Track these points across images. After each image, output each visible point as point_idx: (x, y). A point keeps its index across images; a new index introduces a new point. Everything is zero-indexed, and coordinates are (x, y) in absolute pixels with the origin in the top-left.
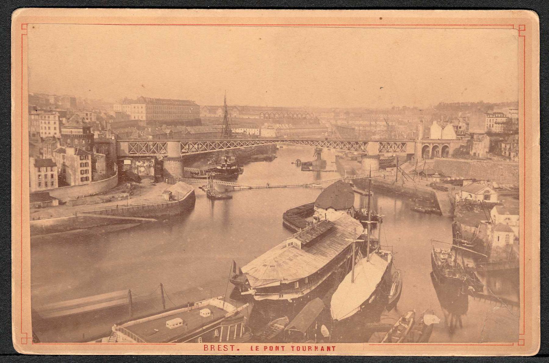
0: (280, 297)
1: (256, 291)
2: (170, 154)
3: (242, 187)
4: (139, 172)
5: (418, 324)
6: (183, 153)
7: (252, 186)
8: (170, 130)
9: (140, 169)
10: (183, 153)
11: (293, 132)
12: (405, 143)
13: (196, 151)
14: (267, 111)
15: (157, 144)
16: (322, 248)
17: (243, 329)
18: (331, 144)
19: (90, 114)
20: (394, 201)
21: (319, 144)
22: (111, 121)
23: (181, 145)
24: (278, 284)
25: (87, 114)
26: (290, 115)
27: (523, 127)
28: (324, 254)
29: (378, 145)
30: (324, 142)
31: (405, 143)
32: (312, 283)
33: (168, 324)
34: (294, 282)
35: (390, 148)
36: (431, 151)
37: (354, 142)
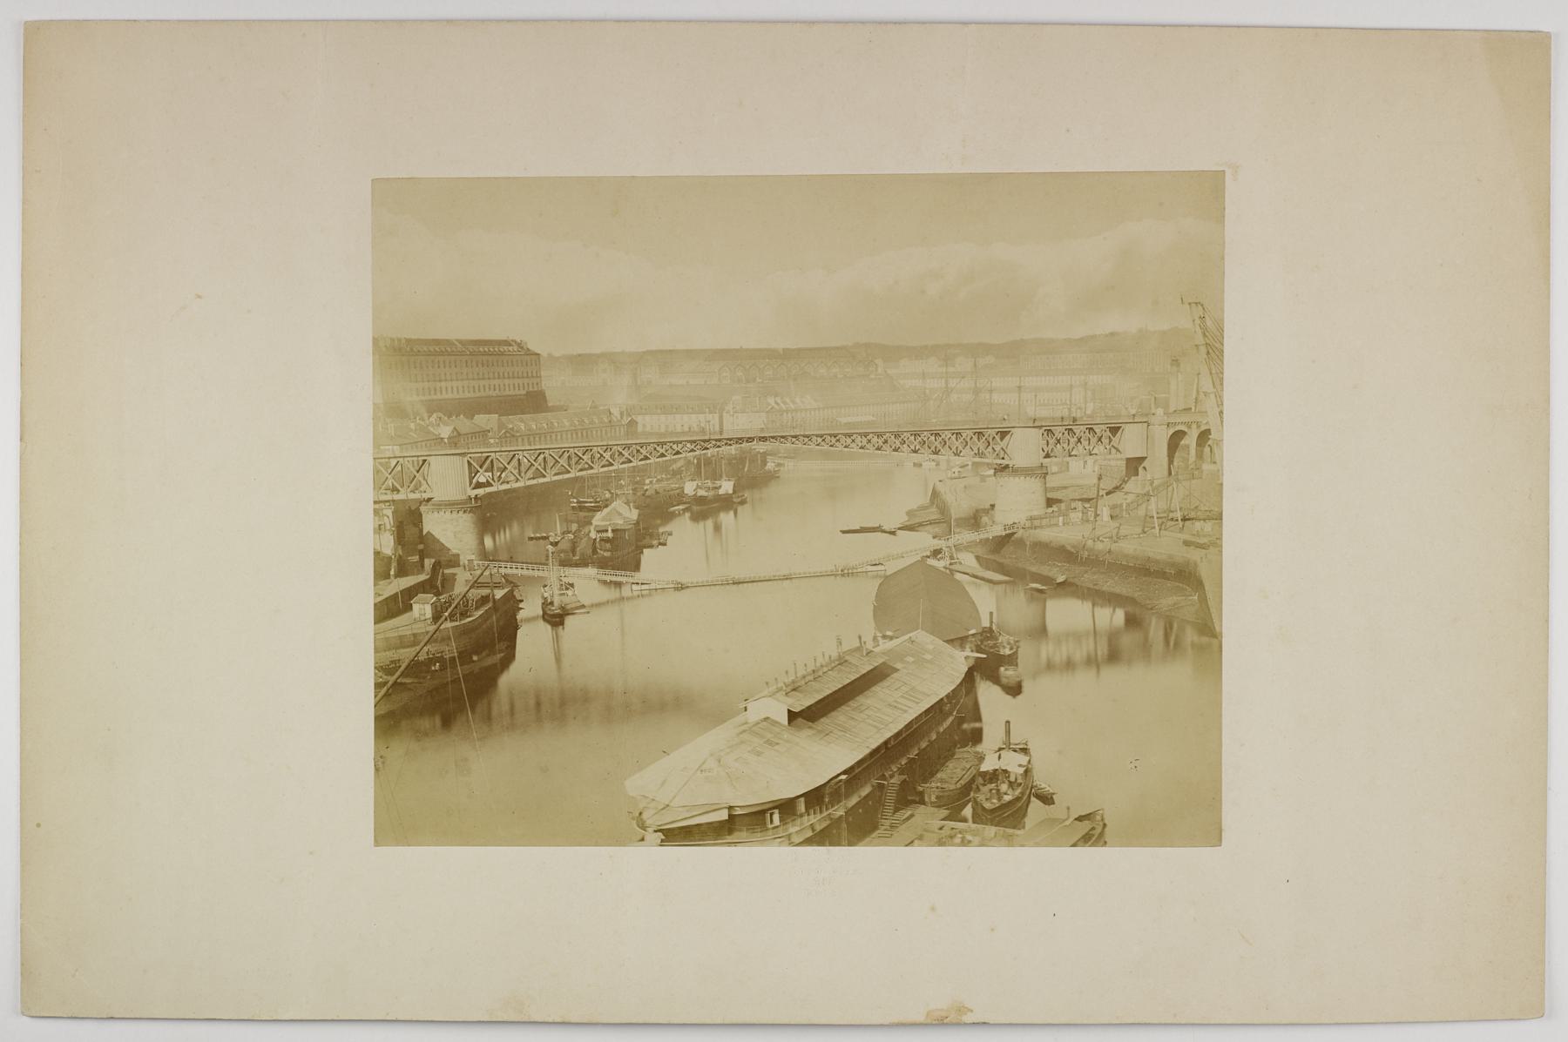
1: (663, 837)
2: (439, 495)
3: (653, 586)
6: (479, 485)
7: (684, 580)
8: (452, 428)
10: (479, 485)
12: (1119, 428)
13: (608, 466)
15: (490, 459)
18: (886, 442)
20: (1111, 610)
21: (869, 441)
23: (468, 461)
24: (724, 815)
29: (1035, 436)
31: (1119, 428)
34: (763, 812)
37: (970, 433)
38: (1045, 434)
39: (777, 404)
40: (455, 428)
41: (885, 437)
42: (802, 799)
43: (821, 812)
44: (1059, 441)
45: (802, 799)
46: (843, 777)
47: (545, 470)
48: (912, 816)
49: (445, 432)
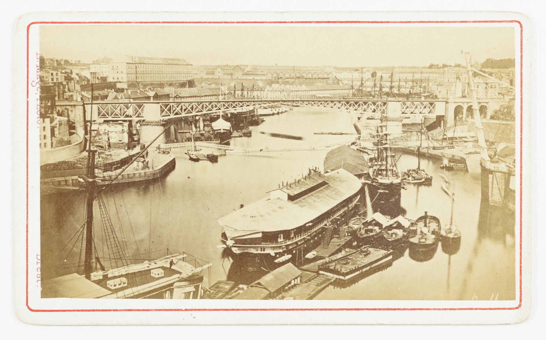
8: (155, 92)
11: (310, 94)
14: (320, 71)
17: (201, 292)
19: (56, 73)
20: (227, 258)
22: (85, 83)
25: (52, 74)
26: (304, 75)
27: (486, 324)
32: (317, 226)
33: (153, 273)
35: (415, 108)
38: (402, 104)
39: (290, 88)
40: (156, 93)
43: (301, 236)
44: (408, 107)
46: (311, 224)
47: (182, 112)
49: (152, 94)
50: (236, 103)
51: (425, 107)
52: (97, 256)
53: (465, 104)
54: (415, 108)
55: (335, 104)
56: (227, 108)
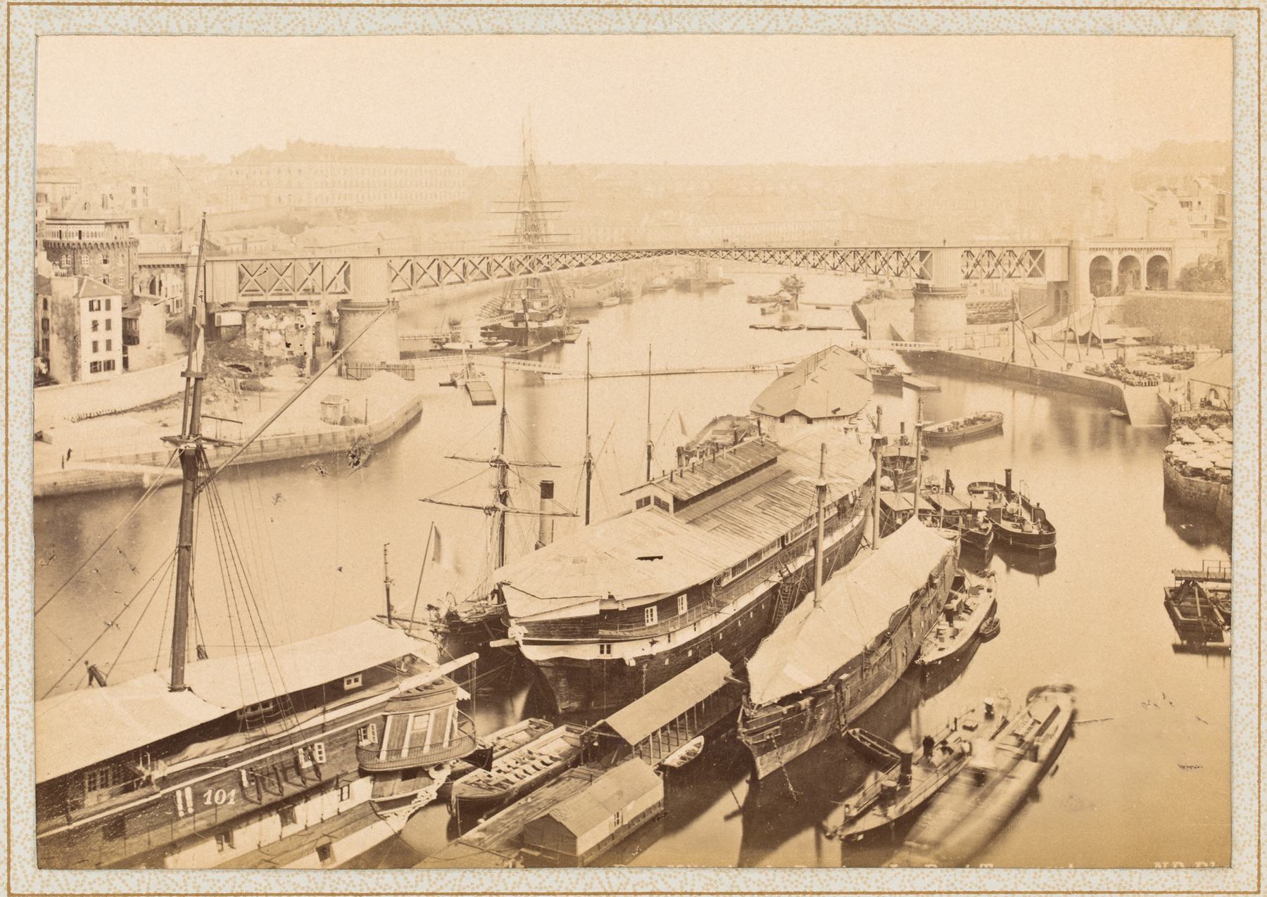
0: (602, 652)
4: (265, 347)
5: (822, 484)
9: (266, 336)
12: (928, 252)
16: (741, 515)
28: (742, 531)
30: (804, 253)
31: (928, 252)
36: (1115, 272)
41: (821, 253)
42: (685, 596)
45: (685, 596)
48: (1057, 768)
50: (569, 258)
51: (1020, 262)
52: (200, 643)
53: (1116, 252)
54: (1017, 265)
55: (805, 258)
56: (548, 269)
